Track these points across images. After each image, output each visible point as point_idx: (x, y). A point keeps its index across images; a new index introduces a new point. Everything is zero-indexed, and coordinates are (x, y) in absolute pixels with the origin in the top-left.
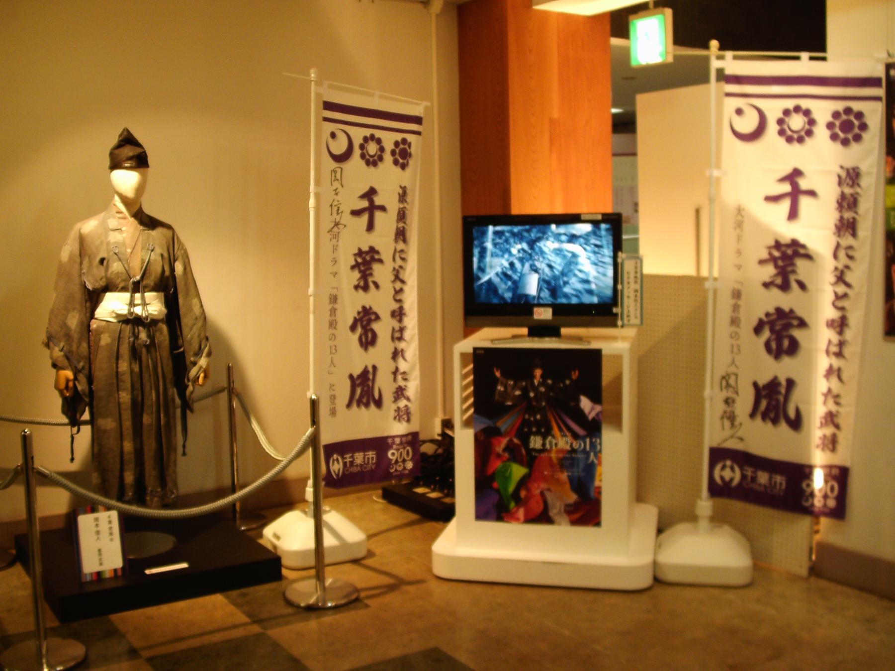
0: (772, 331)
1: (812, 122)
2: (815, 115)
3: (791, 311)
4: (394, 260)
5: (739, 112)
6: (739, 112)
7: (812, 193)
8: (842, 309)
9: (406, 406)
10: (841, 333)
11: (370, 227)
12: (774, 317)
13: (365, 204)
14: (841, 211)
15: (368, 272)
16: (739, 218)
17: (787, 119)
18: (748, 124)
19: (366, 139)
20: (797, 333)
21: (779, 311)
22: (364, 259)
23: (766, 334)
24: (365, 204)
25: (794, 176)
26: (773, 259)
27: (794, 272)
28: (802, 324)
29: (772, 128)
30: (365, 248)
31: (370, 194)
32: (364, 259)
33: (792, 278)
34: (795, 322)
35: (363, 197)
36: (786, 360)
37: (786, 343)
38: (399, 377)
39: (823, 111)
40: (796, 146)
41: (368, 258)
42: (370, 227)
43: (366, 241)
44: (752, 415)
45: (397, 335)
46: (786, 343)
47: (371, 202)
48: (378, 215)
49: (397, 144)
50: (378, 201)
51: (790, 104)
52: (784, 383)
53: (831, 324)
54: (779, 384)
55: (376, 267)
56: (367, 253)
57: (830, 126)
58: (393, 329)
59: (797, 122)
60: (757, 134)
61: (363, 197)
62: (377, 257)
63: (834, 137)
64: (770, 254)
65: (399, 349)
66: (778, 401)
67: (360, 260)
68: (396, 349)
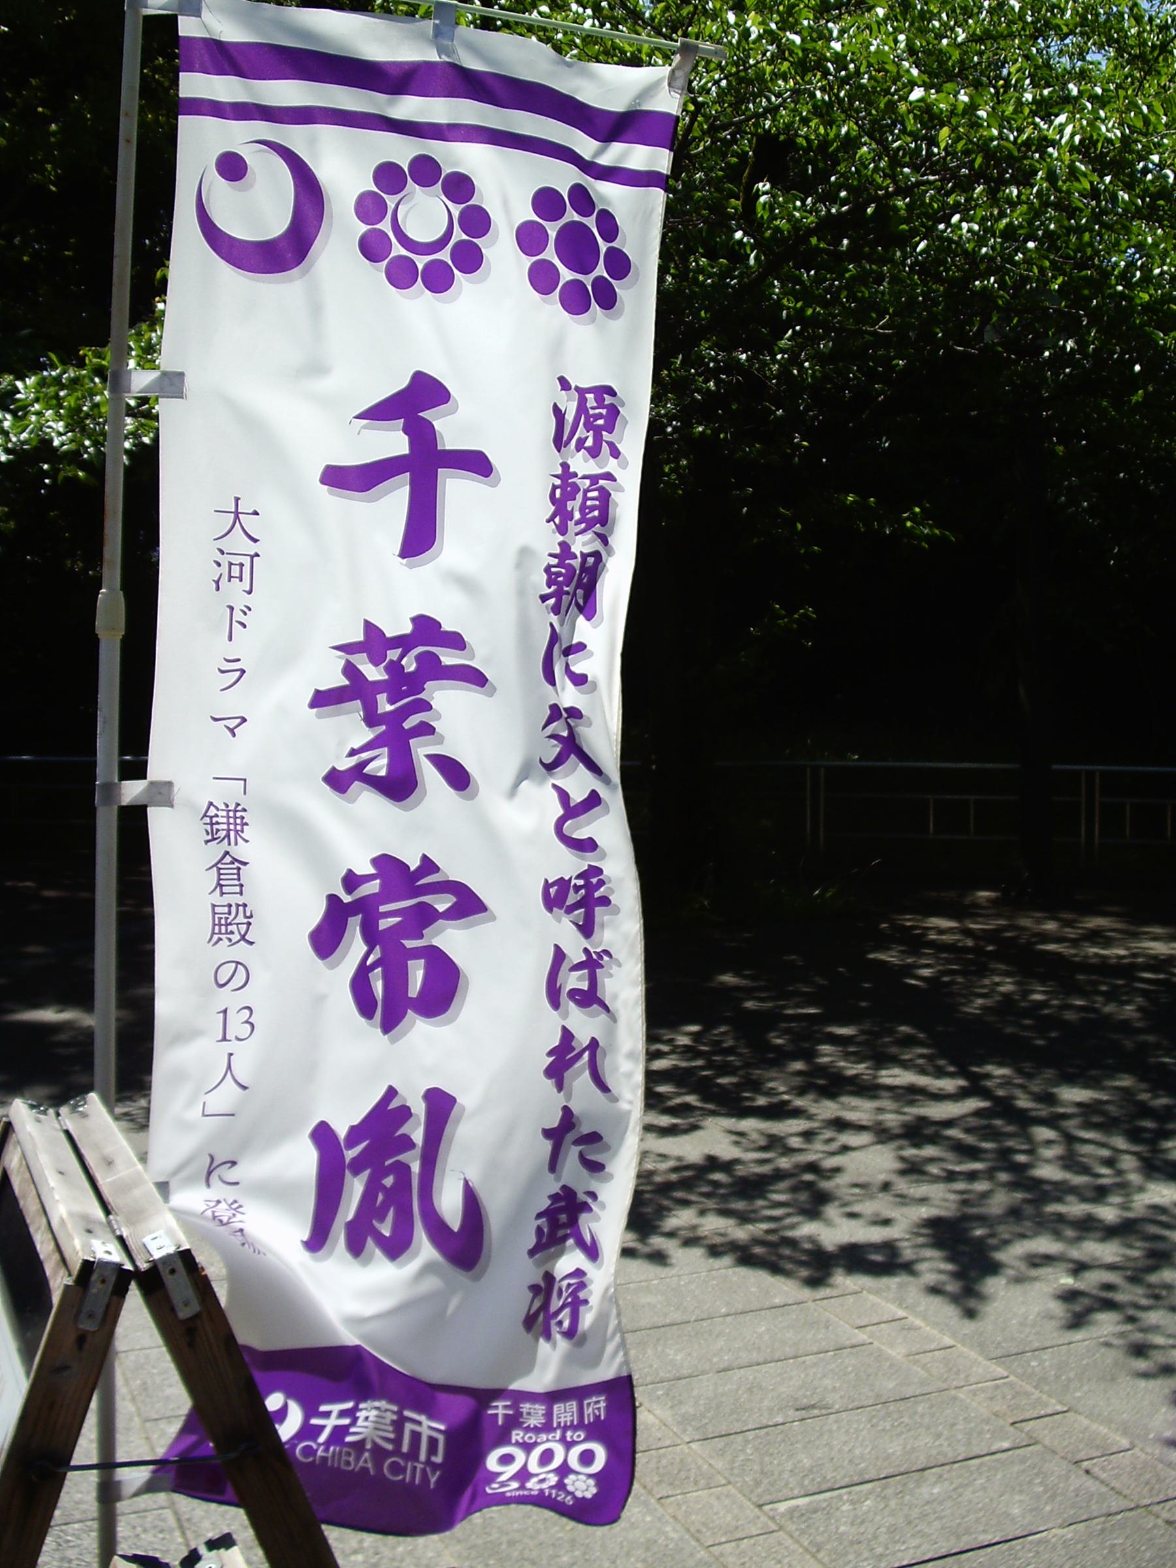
0: (371, 936)
1: (477, 222)
2: (487, 197)
3: (428, 865)
4: (550, 678)
5: (232, 167)
6: (232, 167)
7: (477, 464)
8: (587, 846)
9: (579, 1273)
10: (587, 929)
11: (420, 537)
12: (373, 887)
13: (393, 442)
14: (562, 529)
15: (410, 723)
16: (238, 543)
17: (390, 201)
18: (262, 210)
19: (389, 176)
20: (451, 938)
21: (386, 864)
22: (395, 668)
23: (355, 948)
24: (393, 442)
25: (416, 401)
26: (355, 689)
27: (426, 729)
28: (468, 904)
29: (342, 229)
30: (397, 625)
31: (416, 401)
32: (395, 668)
33: (421, 749)
34: (442, 903)
35: (379, 413)
36: (419, 1030)
37: (417, 974)
38: (572, 1154)
39: (508, 185)
40: (419, 298)
41: (410, 664)
42: (420, 537)
43: (401, 596)
44: (317, 1241)
45: (575, 981)
46: (417, 974)
47: (422, 435)
48: (455, 488)
49: (547, 202)
50: (451, 430)
51: (402, 151)
52: (419, 1108)
53: (556, 896)
54: (405, 1113)
55: (447, 701)
56: (404, 643)
57: (529, 238)
58: (559, 955)
59: (425, 215)
60: (285, 253)
61: (379, 413)
62: (449, 658)
63: (542, 279)
64: (350, 670)
65: (582, 1039)
66: (403, 1170)
67: (373, 673)
68: (567, 1035)
